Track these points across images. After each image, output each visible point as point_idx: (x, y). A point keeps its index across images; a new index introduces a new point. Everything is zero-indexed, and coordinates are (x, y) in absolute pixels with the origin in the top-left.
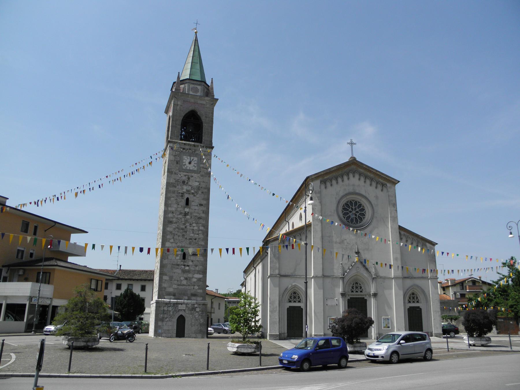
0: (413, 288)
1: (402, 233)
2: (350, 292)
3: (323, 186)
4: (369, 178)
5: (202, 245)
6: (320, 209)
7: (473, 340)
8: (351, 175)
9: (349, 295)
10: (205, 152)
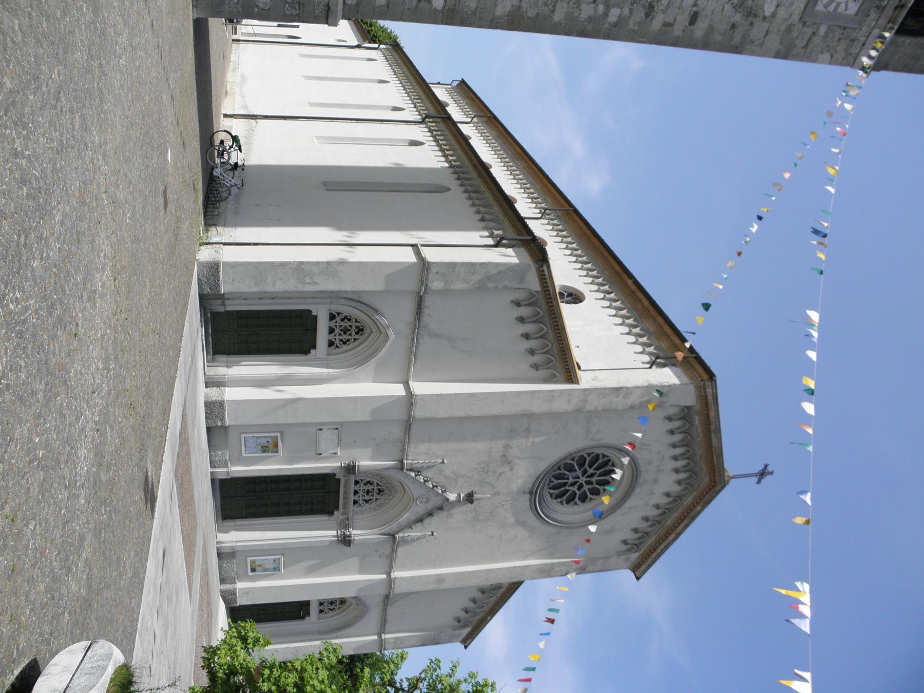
0: (381, 332)
5: (553, 11)
10: (861, 44)
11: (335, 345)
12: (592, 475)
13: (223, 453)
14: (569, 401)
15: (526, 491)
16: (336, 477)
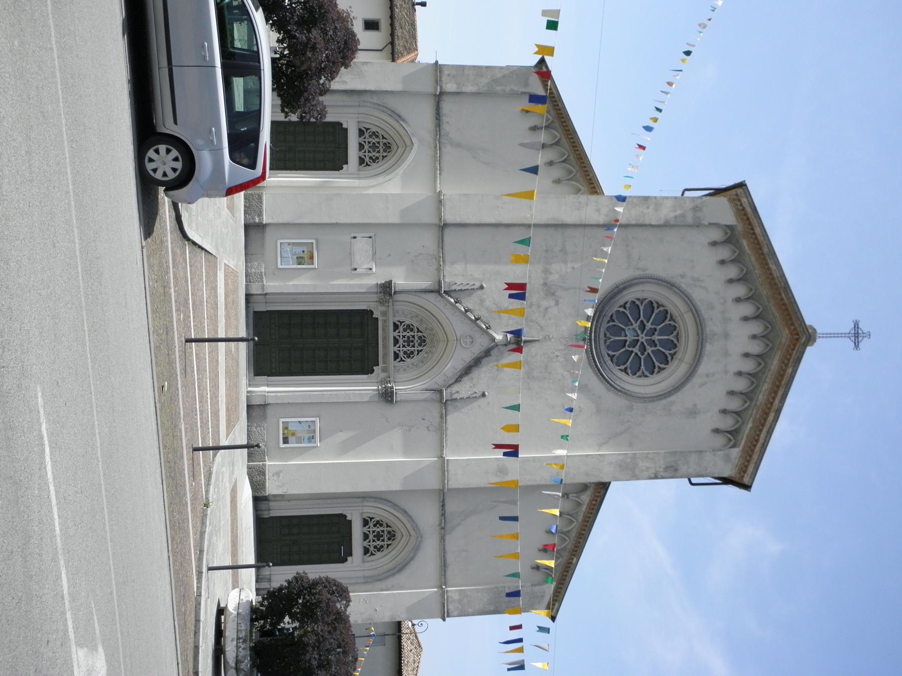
0: (410, 535)
1: (586, 498)
2: (396, 319)
3: (717, 235)
4: (754, 386)
6: (647, 222)
7: (240, 611)
8: (756, 328)
9: (384, 314)
11: (365, 162)
12: (653, 343)
13: (259, 264)
14: (598, 211)
16: (374, 316)
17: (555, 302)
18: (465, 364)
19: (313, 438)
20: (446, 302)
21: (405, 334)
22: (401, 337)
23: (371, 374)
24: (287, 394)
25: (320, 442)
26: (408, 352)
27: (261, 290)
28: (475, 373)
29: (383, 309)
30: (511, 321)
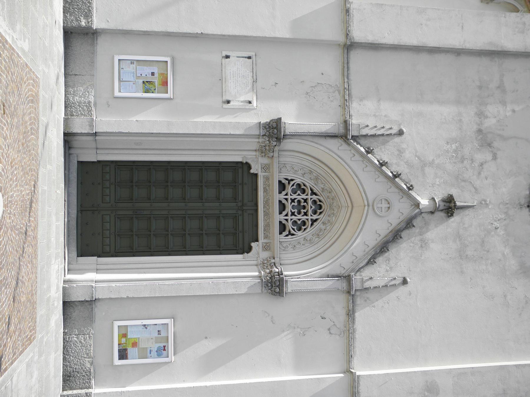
9: (266, 168)
15: (523, 203)
16: (252, 171)
17: (492, 155)
18: (379, 239)
19: (164, 350)
20: (353, 151)
21: (294, 196)
22: (290, 201)
23: (248, 253)
24: (126, 284)
25: (175, 354)
26: (299, 222)
27: (88, 127)
28: (393, 251)
29: (265, 161)
30: (438, 180)
